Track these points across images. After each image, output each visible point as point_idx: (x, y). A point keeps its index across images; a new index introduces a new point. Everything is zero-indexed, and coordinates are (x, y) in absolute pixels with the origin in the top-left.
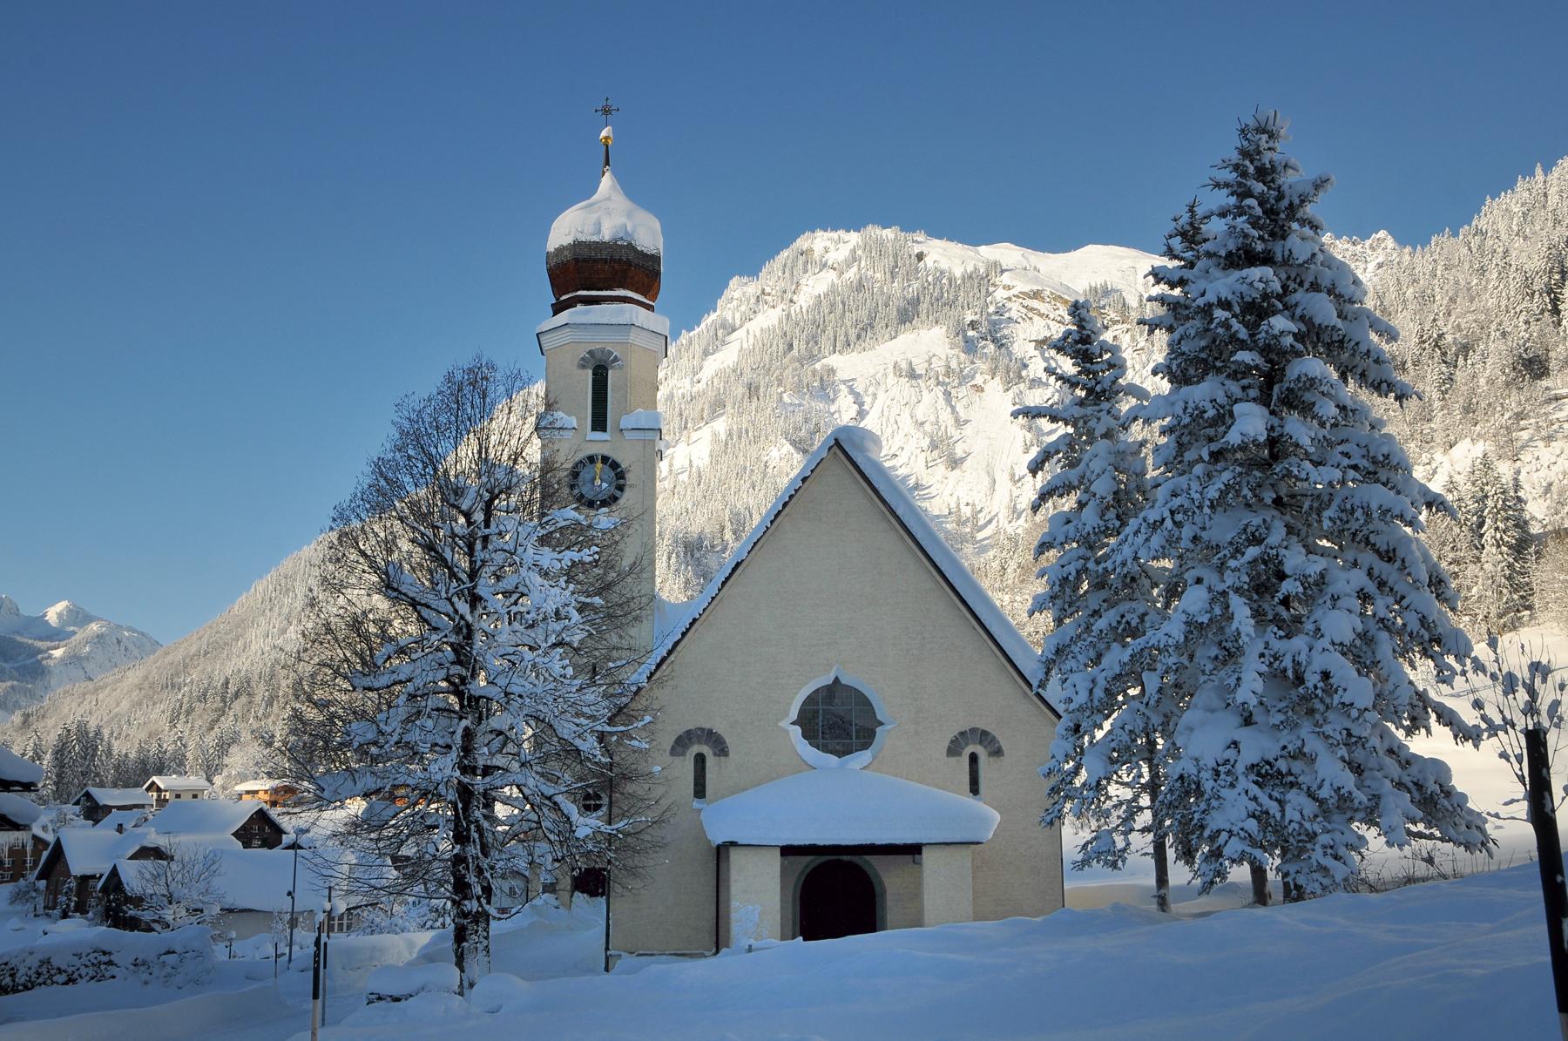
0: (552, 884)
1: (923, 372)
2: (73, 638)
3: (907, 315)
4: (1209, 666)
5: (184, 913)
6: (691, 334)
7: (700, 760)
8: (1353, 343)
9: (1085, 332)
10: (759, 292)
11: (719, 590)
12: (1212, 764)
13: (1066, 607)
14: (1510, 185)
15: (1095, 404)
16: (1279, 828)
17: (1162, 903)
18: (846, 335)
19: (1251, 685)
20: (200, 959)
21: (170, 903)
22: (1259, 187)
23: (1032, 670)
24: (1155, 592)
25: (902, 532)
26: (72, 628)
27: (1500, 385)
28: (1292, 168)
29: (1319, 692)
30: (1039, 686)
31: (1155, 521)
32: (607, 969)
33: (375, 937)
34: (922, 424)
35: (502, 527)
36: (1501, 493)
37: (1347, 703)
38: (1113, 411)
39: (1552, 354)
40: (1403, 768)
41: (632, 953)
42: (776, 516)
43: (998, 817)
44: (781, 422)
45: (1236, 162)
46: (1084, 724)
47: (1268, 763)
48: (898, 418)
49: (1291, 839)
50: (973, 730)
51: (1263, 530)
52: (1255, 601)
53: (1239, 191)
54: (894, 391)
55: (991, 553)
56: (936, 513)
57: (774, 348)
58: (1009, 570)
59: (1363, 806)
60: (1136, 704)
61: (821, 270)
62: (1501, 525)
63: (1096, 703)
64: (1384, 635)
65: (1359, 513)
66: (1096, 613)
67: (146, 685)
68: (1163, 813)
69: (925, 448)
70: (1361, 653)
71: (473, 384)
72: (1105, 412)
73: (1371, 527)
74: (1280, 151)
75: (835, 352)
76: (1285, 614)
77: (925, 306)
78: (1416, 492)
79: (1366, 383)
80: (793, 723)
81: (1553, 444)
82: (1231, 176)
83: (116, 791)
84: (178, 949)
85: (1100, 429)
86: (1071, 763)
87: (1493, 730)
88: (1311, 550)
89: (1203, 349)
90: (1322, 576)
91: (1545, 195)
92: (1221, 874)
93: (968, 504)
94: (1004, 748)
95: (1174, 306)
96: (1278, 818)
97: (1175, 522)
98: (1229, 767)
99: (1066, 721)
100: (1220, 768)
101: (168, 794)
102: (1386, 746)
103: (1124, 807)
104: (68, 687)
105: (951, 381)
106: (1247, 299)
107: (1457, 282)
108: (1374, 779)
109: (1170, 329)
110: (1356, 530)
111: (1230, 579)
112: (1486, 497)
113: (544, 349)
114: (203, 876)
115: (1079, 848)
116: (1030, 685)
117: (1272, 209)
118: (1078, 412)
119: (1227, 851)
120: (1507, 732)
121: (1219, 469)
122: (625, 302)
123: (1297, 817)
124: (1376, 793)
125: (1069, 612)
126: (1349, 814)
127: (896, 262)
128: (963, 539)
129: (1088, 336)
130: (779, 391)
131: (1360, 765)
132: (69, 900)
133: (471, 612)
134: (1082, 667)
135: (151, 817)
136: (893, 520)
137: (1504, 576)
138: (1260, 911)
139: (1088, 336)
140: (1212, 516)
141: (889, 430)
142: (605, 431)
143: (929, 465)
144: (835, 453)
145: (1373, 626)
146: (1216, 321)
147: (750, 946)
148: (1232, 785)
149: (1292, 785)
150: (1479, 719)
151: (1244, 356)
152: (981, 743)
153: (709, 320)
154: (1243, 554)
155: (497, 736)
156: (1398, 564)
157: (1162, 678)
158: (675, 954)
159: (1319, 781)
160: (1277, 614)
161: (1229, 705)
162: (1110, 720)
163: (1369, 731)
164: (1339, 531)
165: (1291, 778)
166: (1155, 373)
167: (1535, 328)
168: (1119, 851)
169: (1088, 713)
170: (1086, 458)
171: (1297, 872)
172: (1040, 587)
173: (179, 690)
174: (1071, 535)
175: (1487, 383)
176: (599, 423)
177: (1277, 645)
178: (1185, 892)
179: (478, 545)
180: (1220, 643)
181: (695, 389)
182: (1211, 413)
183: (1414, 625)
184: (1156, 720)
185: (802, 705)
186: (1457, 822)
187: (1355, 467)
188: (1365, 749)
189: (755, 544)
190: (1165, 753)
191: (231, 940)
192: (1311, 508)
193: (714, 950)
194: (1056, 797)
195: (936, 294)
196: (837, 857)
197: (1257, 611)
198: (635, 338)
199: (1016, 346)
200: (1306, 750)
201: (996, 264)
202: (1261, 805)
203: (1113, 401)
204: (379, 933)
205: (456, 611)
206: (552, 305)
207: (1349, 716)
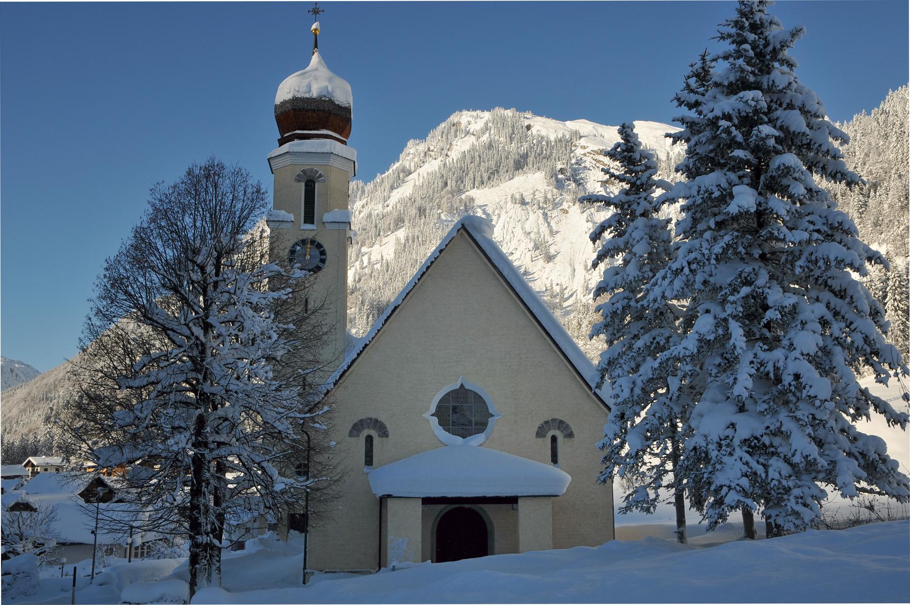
0: (274, 524)
1: (530, 201)
3: (520, 164)
4: (714, 371)
5: (30, 546)
6: (383, 176)
7: (369, 439)
8: (817, 145)
9: (629, 144)
10: (426, 150)
11: (383, 325)
12: (716, 439)
13: (615, 332)
15: (636, 194)
16: (764, 484)
17: (681, 536)
18: (481, 177)
19: (744, 383)
20: (29, 578)
22: (752, 37)
23: (593, 380)
24: (677, 323)
25: (507, 287)
28: (775, 24)
29: (792, 388)
31: (677, 269)
32: (304, 583)
33: (161, 560)
34: (529, 233)
35: (225, 276)
36: (898, 277)
37: (812, 396)
38: (648, 198)
40: (851, 441)
41: (322, 571)
42: (422, 275)
43: (569, 478)
44: (440, 232)
45: (736, 19)
46: (627, 413)
47: (756, 438)
48: (514, 230)
49: (773, 492)
50: (554, 420)
51: (752, 276)
52: (747, 325)
53: (738, 39)
54: (511, 213)
55: (572, 316)
56: (538, 290)
57: (436, 185)
58: (583, 326)
59: (824, 469)
60: (663, 399)
61: (465, 136)
62: (898, 297)
63: (635, 398)
64: (838, 349)
65: (821, 263)
66: (636, 337)
67: (29, 398)
68: (682, 474)
71: (207, 177)
72: (643, 199)
73: (829, 273)
75: (474, 188)
76: (768, 334)
77: (531, 159)
78: (861, 249)
79: (826, 174)
80: (433, 415)
82: (733, 31)
85: (639, 211)
86: (619, 440)
88: (785, 290)
89: (711, 151)
90: (794, 307)
92: (723, 517)
93: (557, 284)
94: (574, 432)
95: (692, 126)
97: (691, 270)
98: (728, 441)
100: (722, 442)
101: (39, 468)
102: (840, 427)
103: (655, 470)
105: (547, 207)
106: (743, 114)
107: (870, 144)
108: (831, 450)
109: (687, 141)
110: (818, 277)
111: (729, 309)
112: (888, 279)
113: (273, 169)
114: (44, 521)
115: (624, 499)
118: (624, 198)
119: (727, 500)
121: (722, 234)
122: (327, 138)
123: (777, 476)
124: (833, 460)
126: (813, 475)
127: (513, 131)
128: (555, 307)
129: (632, 147)
130: (438, 212)
131: (821, 440)
133: (205, 335)
134: (626, 373)
136: (501, 279)
137: (900, 330)
138: (749, 542)
139: (632, 147)
140: (717, 266)
141: (508, 237)
142: (313, 223)
143: (533, 259)
144: (462, 234)
145: (830, 342)
146: (721, 128)
148: (731, 454)
149: (773, 454)
151: (739, 153)
152: (559, 428)
153: (394, 167)
154: (738, 292)
155: (224, 421)
156: (848, 299)
157: (681, 381)
158: (351, 572)
159: (793, 450)
160: (762, 334)
161: (728, 398)
162: (646, 410)
163: (828, 416)
164: (806, 277)
165: (772, 449)
168: (652, 500)
169: (630, 405)
170: (629, 230)
171: (777, 515)
172: (598, 318)
173: (51, 401)
175: (889, 207)
176: (309, 217)
177: (762, 355)
178: (696, 530)
179: (210, 288)
180: (722, 355)
181: (385, 211)
182: (717, 194)
183: (859, 342)
184: (677, 409)
185: (439, 403)
186: (891, 481)
188: (825, 428)
189: (407, 294)
190: (683, 432)
191: (63, 564)
192: (786, 260)
195: (538, 151)
196: (462, 505)
197: (748, 332)
198: (335, 163)
199: (589, 184)
200: (783, 429)
202: (751, 468)
203: (649, 191)
204: (163, 558)
205: (192, 334)
207: (814, 405)
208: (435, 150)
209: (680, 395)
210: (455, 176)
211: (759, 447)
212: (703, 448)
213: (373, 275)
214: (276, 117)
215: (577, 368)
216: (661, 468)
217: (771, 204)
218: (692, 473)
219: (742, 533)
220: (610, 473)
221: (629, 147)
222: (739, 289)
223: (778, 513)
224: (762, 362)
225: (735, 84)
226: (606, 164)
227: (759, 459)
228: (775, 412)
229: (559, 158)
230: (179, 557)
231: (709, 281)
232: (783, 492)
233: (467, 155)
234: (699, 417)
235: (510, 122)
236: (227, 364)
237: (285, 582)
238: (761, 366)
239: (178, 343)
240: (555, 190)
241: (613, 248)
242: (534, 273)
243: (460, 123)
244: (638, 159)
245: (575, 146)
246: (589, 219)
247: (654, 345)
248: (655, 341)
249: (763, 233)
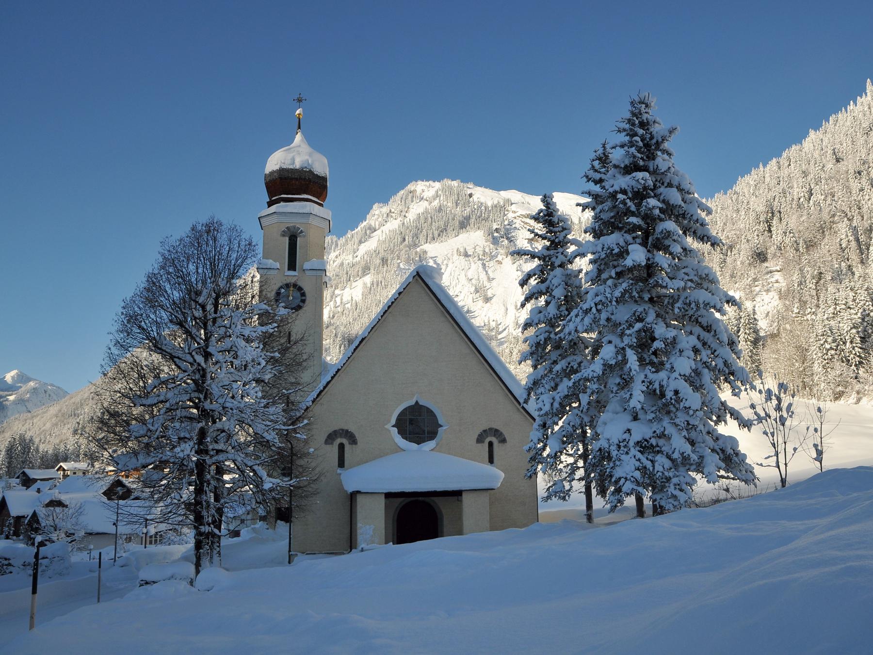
2: (20, 390)
3: (464, 224)
4: (615, 389)
5: (63, 535)
6: (353, 232)
7: (341, 447)
8: (689, 215)
9: (550, 210)
11: (352, 353)
13: (539, 358)
14: (749, 172)
15: (555, 249)
17: (589, 518)
18: (433, 234)
19: (638, 397)
21: (56, 530)
22: (641, 132)
23: (521, 395)
24: (587, 351)
25: (452, 322)
26: (19, 385)
27: (746, 265)
29: (673, 401)
30: (524, 402)
31: (587, 309)
32: (289, 563)
33: (172, 546)
34: (471, 280)
35: (222, 313)
36: (748, 316)
38: (565, 253)
39: (769, 251)
40: (714, 441)
41: (303, 553)
42: (384, 313)
43: (503, 475)
46: (548, 422)
47: (646, 440)
48: (459, 277)
49: (658, 481)
50: (491, 429)
52: (639, 353)
53: (631, 133)
55: (505, 346)
56: (478, 325)
57: (396, 240)
58: (514, 354)
60: (576, 411)
61: (420, 201)
62: (748, 332)
63: (555, 411)
64: (706, 371)
65: (693, 305)
66: (555, 362)
67: (60, 414)
69: (472, 292)
70: (694, 380)
71: (208, 232)
73: (699, 313)
74: (651, 114)
76: (655, 360)
77: (473, 220)
79: (696, 237)
80: (393, 426)
81: (769, 293)
82: (627, 126)
83: (40, 471)
84: (50, 556)
85: (557, 263)
86: (542, 444)
87: (760, 419)
88: (668, 325)
89: (612, 218)
90: (674, 338)
91: (764, 177)
92: (621, 501)
93: (494, 321)
95: (596, 197)
96: (651, 470)
97: (597, 310)
98: (625, 443)
99: (539, 421)
100: (621, 444)
101: (69, 472)
102: (706, 430)
103: (569, 467)
104: (17, 416)
105: (486, 259)
106: (636, 190)
107: (727, 216)
108: (700, 447)
109: (593, 209)
111: (626, 340)
112: (741, 318)
116: (519, 403)
117: (648, 144)
118: (546, 253)
119: (624, 489)
120: (767, 421)
121: (620, 282)
123: (661, 469)
125: (541, 361)
126: (688, 467)
127: (459, 198)
128: (491, 338)
129: (552, 212)
132: (10, 529)
134: (547, 391)
135: (58, 484)
136: (448, 316)
137: (749, 356)
138: (640, 520)
139: (552, 212)
142: (295, 271)
145: (700, 366)
146: (619, 200)
147: (362, 548)
148: (627, 453)
149: (658, 452)
150: (753, 414)
151: (633, 220)
152: (495, 436)
153: (362, 225)
154: (633, 327)
155: (222, 432)
156: (713, 333)
157: (590, 397)
158: (328, 553)
159: (673, 449)
160: (651, 360)
162: (563, 420)
165: (658, 449)
166: (586, 232)
167: (761, 238)
168: (567, 491)
170: (550, 278)
171: (661, 499)
172: (525, 347)
173: (78, 417)
174: (542, 319)
176: (292, 266)
177: (651, 376)
178: (601, 512)
179: (210, 323)
180: (621, 376)
181: (355, 261)
182: (616, 250)
183: (721, 365)
184: (586, 419)
187: (691, 281)
189: (372, 328)
192: (668, 302)
193: (349, 550)
194: (533, 463)
196: (416, 498)
198: (313, 221)
199: (518, 241)
200: (666, 433)
201: (508, 200)
202: (642, 464)
203: (565, 247)
205: (195, 361)
206: (267, 202)
207: (688, 414)
208: (396, 212)
209: (589, 408)
211: (648, 447)
217: (657, 259)
219: (635, 513)
220: (535, 470)
223: (662, 497)
232: (665, 481)
243: (416, 191)
245: (508, 211)
249: (651, 282)
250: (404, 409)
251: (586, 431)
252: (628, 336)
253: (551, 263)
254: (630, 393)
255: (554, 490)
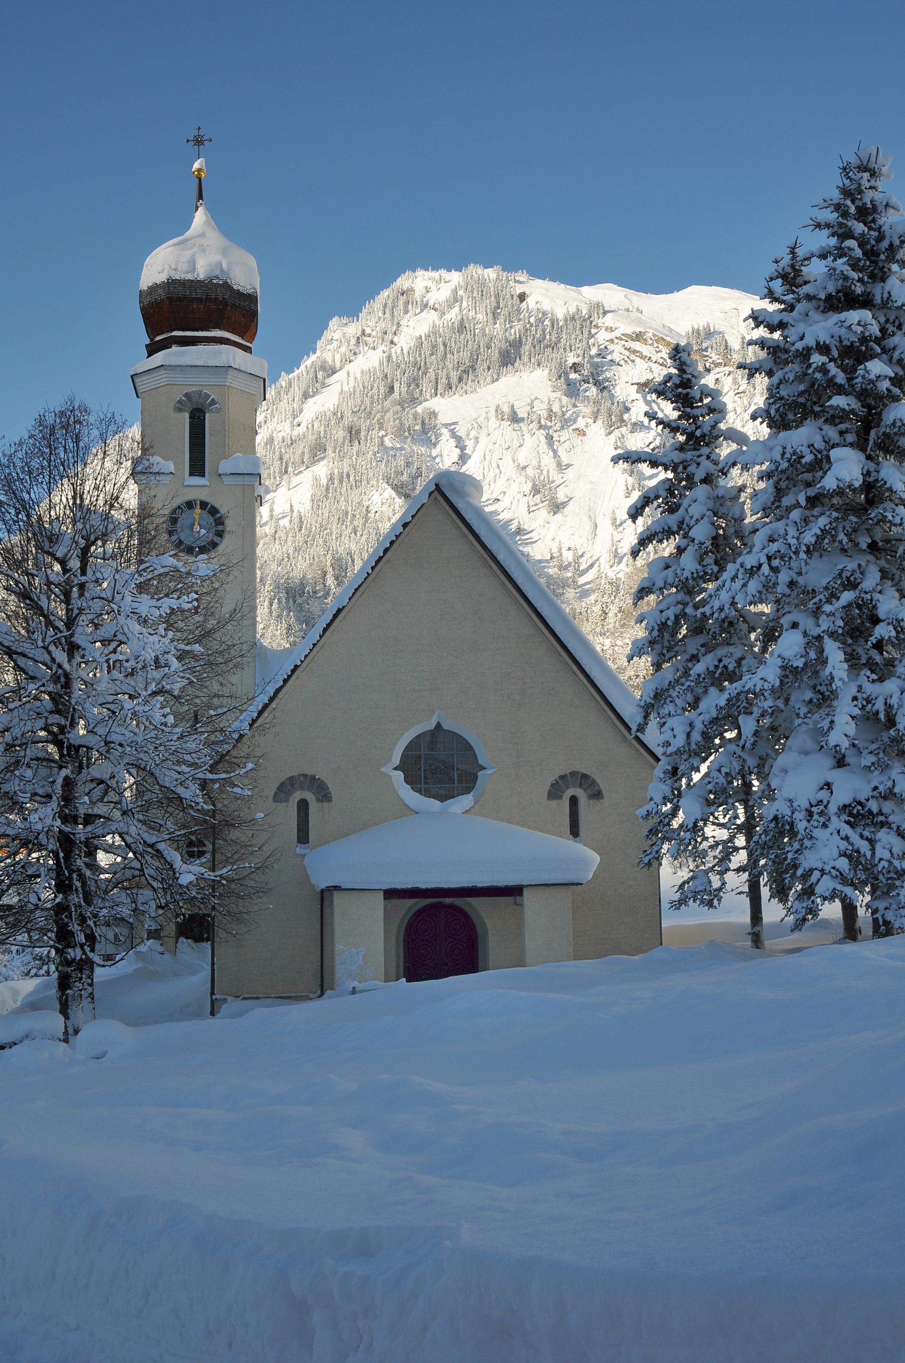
1: (525, 416)
6: (291, 376)
7: (303, 806)
9: (685, 376)
10: (359, 333)
13: (665, 651)
15: (695, 449)
16: (869, 866)
17: (757, 940)
18: (448, 377)
22: (859, 228)
23: (632, 715)
24: (753, 636)
31: (752, 567)
32: (212, 1013)
34: (524, 468)
35: (99, 575)
38: (713, 456)
42: (377, 562)
43: (596, 858)
44: (383, 467)
46: (682, 768)
47: (860, 803)
49: (881, 877)
50: (573, 774)
51: (858, 575)
52: (849, 645)
53: (840, 231)
55: (592, 598)
56: (538, 557)
57: (375, 390)
58: (610, 615)
60: (732, 747)
61: (422, 311)
63: (693, 746)
66: (695, 658)
69: (527, 492)
71: (66, 427)
72: (704, 457)
76: (878, 658)
77: (527, 348)
80: (396, 769)
85: (700, 474)
89: (801, 394)
92: (813, 911)
93: (569, 549)
95: (774, 350)
97: (772, 568)
98: (821, 807)
99: (664, 764)
100: (813, 809)
103: (720, 847)
106: (846, 343)
109: (770, 374)
111: (825, 623)
113: (140, 391)
115: (676, 888)
116: (629, 729)
117: (872, 250)
118: (677, 456)
119: (819, 889)
122: (222, 344)
123: (887, 855)
125: (668, 656)
127: (498, 303)
128: (565, 584)
129: (689, 380)
130: (380, 434)
133: (69, 661)
134: (679, 711)
138: (850, 948)
139: (689, 380)
140: (808, 561)
142: (204, 476)
143: (531, 509)
144: (436, 498)
146: (814, 366)
148: (825, 826)
149: (882, 824)
151: (840, 401)
152: (581, 786)
154: (838, 599)
155: (98, 785)
157: (758, 721)
158: (280, 997)
160: (870, 658)
161: (822, 747)
162: (707, 763)
165: (881, 818)
166: (754, 417)
168: (715, 890)
169: (685, 757)
170: (685, 503)
171: (886, 908)
172: (640, 632)
176: (197, 467)
178: (778, 929)
180: (814, 687)
181: (295, 433)
182: (808, 458)
184: (751, 762)
189: (356, 590)
193: (319, 992)
195: (538, 336)
197: (851, 655)
198: (232, 380)
199: (618, 389)
200: (896, 790)
202: (852, 845)
203: (713, 446)
205: (53, 660)
206: (147, 346)
208: (374, 333)
209: (756, 741)
210: (406, 375)
211: (863, 815)
212: (786, 817)
213: (277, 536)
214: (142, 309)
215: (604, 693)
216: (729, 844)
217: (883, 474)
218: (771, 852)
219: (841, 932)
220: (657, 852)
221: (685, 380)
222: (839, 595)
223: (888, 905)
224: (868, 698)
225: (836, 296)
226: (646, 357)
227: (864, 833)
228: (885, 768)
229: (571, 346)
230: (6, 980)
231: (797, 582)
232: (895, 876)
233: (425, 342)
234: (782, 774)
235: (492, 289)
236: (104, 703)
237: (186, 1013)
238: (868, 703)
239: (31, 673)
240: (565, 398)
241: (661, 530)
242: (532, 531)
243: (413, 290)
244: (698, 397)
245: (596, 327)
246: (619, 444)
247: (719, 671)
248: (721, 666)
249: (873, 515)
250: (416, 737)
251: (750, 782)
252: (828, 616)
253: (687, 475)
254: (829, 719)
255: (692, 889)
